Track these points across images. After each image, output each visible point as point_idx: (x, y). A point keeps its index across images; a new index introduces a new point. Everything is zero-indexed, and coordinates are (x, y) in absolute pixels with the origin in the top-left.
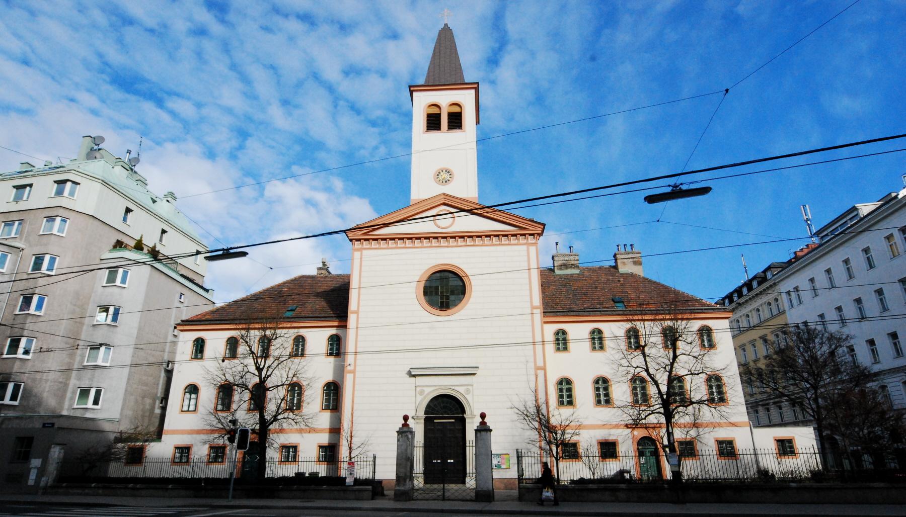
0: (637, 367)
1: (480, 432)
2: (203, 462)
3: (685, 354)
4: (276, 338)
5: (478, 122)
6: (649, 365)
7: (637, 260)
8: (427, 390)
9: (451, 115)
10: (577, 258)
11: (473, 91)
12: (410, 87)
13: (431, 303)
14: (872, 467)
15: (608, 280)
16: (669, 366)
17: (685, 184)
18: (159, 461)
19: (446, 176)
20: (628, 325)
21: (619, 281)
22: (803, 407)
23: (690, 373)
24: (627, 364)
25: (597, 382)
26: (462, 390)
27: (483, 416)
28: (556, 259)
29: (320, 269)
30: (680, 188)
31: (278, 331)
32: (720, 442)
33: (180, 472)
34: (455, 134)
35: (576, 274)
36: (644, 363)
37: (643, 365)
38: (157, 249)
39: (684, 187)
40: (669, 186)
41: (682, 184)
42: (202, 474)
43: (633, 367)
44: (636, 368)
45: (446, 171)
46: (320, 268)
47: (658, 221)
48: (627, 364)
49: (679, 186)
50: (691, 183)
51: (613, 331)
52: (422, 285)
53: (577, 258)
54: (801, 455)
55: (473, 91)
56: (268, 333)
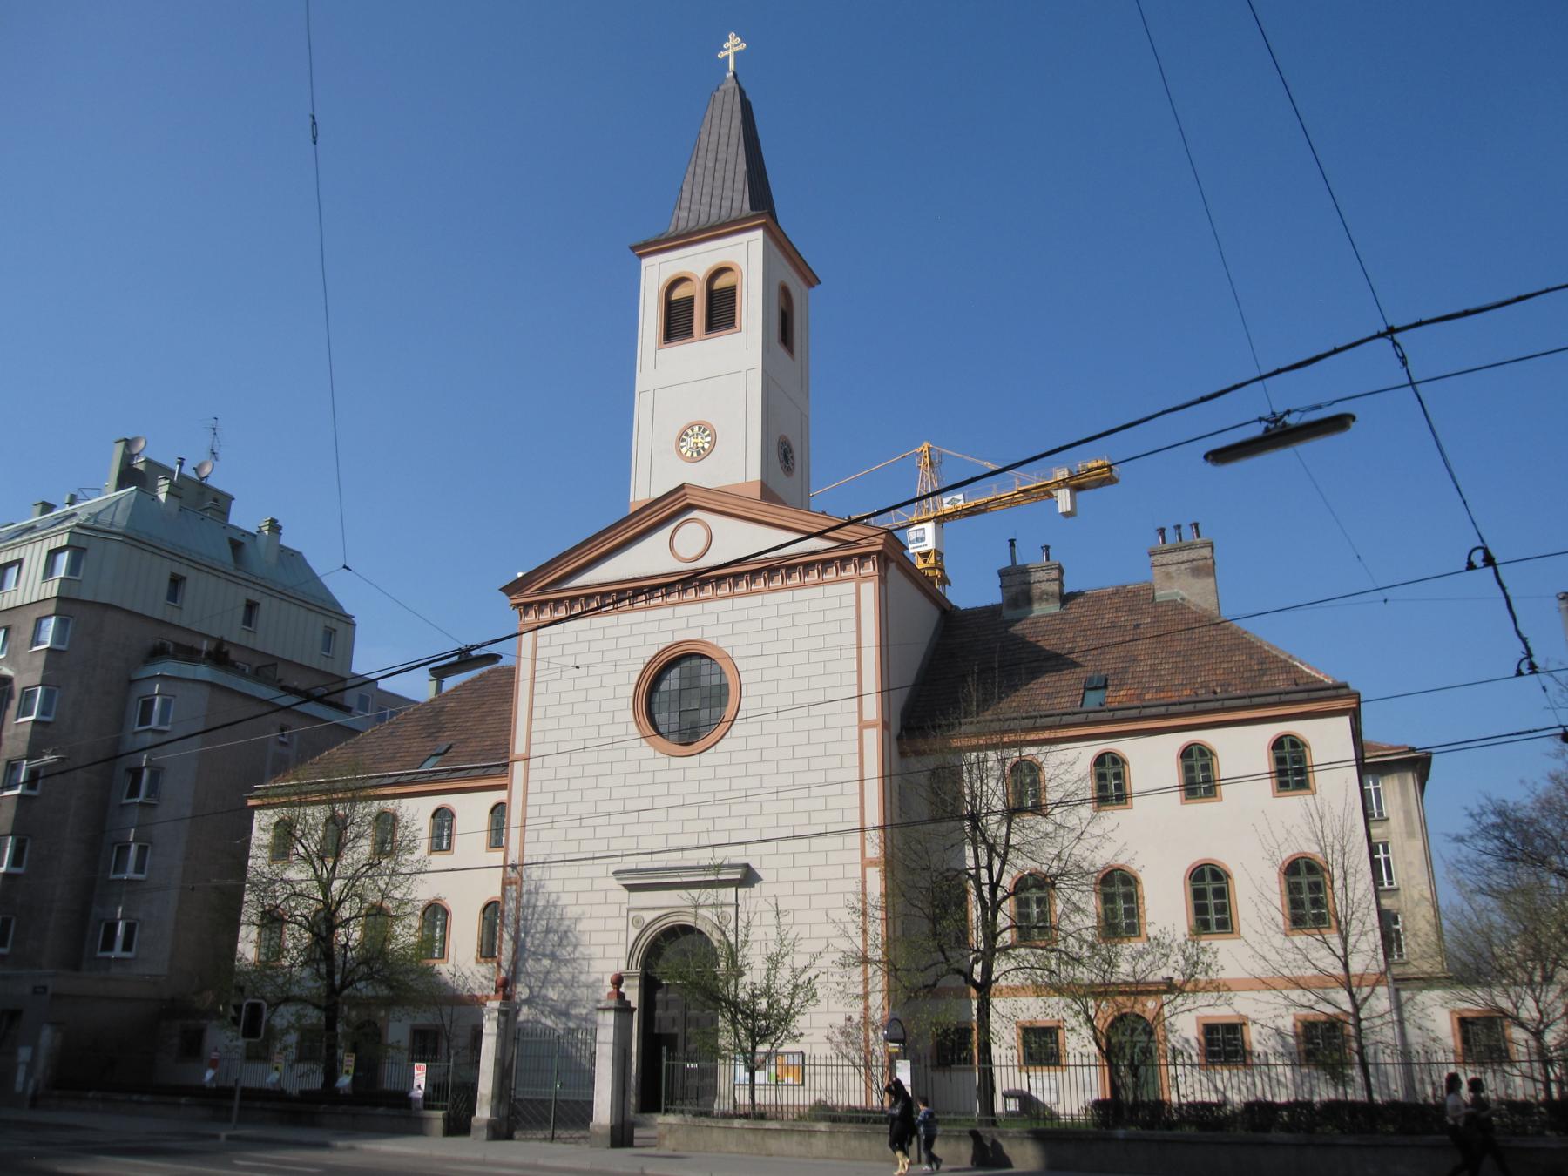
7: (1201, 562)
8: (649, 916)
9: (712, 295)
11: (1345, 721)
18: (818, 1062)
19: (703, 441)
32: (1210, 1030)
33: (829, 1078)
34: (722, 342)
39: (1292, 420)
40: (1260, 419)
41: (1288, 412)
49: (1282, 417)
54: (1072, 1069)
55: (1345, 721)
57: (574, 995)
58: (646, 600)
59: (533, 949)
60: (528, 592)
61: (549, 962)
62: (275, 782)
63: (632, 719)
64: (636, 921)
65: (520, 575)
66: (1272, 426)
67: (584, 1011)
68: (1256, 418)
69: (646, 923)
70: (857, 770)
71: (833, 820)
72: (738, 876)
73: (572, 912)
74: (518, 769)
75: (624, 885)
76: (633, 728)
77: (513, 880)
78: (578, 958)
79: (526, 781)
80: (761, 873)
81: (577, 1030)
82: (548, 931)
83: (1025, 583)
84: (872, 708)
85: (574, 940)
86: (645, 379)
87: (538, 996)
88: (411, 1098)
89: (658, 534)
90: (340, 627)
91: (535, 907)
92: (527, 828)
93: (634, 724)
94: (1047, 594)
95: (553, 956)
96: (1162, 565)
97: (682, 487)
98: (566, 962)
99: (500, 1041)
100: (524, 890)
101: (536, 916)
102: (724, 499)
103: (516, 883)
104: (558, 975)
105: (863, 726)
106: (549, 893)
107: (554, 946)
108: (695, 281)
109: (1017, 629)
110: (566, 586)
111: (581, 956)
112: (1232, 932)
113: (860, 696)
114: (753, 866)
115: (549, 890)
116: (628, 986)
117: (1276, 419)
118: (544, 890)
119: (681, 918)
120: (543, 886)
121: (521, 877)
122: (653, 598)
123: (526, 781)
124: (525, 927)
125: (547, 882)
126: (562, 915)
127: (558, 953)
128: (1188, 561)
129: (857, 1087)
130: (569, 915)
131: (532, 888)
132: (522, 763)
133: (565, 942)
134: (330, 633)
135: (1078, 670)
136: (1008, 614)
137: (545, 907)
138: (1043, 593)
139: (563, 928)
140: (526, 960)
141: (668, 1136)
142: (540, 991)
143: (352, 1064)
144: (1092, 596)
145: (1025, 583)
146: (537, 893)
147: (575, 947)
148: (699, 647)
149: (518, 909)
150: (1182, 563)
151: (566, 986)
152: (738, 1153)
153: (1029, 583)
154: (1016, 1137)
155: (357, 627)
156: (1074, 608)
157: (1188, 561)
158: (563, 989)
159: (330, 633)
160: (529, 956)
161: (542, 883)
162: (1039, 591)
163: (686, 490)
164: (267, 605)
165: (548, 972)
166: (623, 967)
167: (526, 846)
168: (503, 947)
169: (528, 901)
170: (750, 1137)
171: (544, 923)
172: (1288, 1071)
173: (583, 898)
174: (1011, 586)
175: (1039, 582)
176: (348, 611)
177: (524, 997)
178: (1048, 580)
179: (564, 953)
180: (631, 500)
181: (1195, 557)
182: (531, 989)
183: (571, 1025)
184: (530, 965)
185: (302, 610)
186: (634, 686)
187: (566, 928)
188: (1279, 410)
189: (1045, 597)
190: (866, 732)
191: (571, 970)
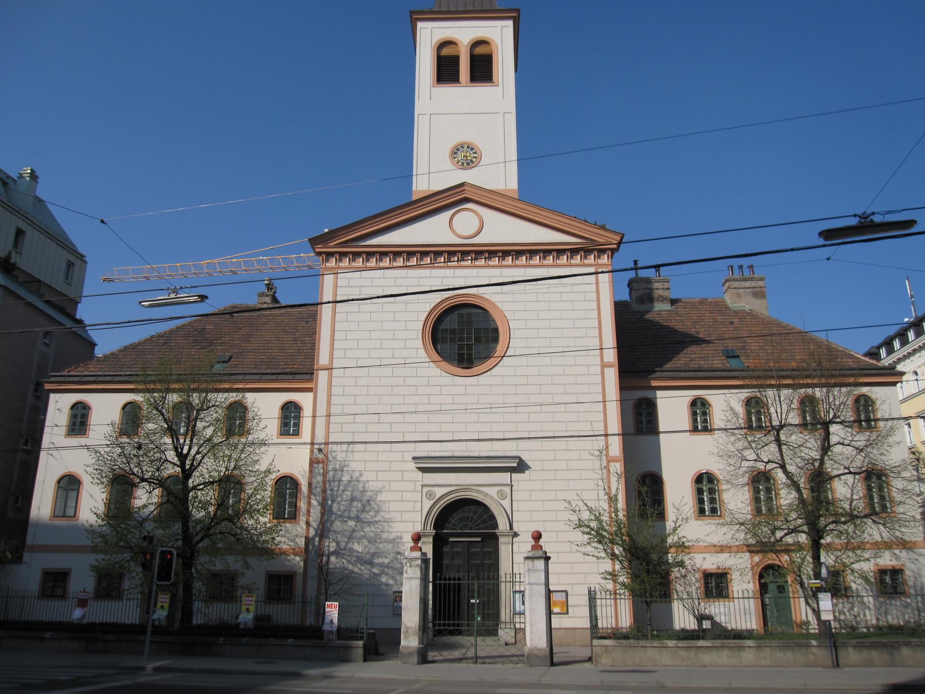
0: (769, 461)
1: (533, 561)
2: (31, 597)
3: (842, 444)
5: (516, 70)
7: (758, 290)
8: (440, 492)
9: (473, 58)
12: (412, 13)
13: (445, 356)
15: (715, 321)
16: (818, 461)
17: (877, 213)
20: (745, 394)
21: (732, 323)
23: (846, 471)
24: (754, 457)
25: (699, 479)
26: (493, 492)
27: (537, 536)
29: (262, 295)
30: (872, 219)
34: (481, 91)
35: (665, 311)
36: (778, 455)
38: (12, 261)
39: (877, 219)
40: (855, 216)
41: (873, 214)
42: (116, 616)
43: (763, 461)
44: (767, 463)
45: (468, 147)
48: (754, 457)
49: (869, 216)
50: (888, 212)
52: (500, 348)
56: (195, 399)
57: (378, 548)
58: (458, 261)
59: (339, 513)
60: (332, 244)
61: (354, 523)
62: (69, 372)
64: (430, 495)
65: (326, 230)
67: (386, 561)
69: (437, 497)
71: (586, 429)
73: (372, 486)
74: (322, 376)
76: (422, 353)
77: (320, 460)
78: (380, 521)
80: (529, 463)
81: (379, 575)
82: (353, 499)
83: (648, 289)
84: (611, 356)
85: (375, 507)
86: (421, 105)
87: (345, 549)
88: (323, 631)
89: (428, 220)
90: (77, 262)
91: (340, 481)
94: (662, 297)
95: (357, 519)
97: (462, 185)
98: (369, 523)
99: (422, 582)
100: (330, 468)
101: (341, 488)
102: (503, 200)
103: (323, 463)
104: (362, 533)
105: (604, 366)
106: (353, 471)
107: (358, 511)
108: (460, 45)
109: (648, 316)
110: (363, 244)
111: (382, 520)
112: (720, 516)
113: (601, 349)
114: (523, 458)
116: (423, 543)
118: (348, 469)
119: (467, 493)
120: (347, 466)
121: (327, 458)
122: (463, 260)
124: (332, 496)
125: (350, 463)
126: (364, 487)
127: (362, 516)
129: (609, 615)
130: (371, 488)
131: (337, 466)
132: (326, 372)
133: (367, 509)
134: (70, 265)
135: (711, 345)
136: (636, 307)
137: (349, 482)
138: (660, 296)
139: (366, 498)
140: (333, 522)
141: (604, 655)
142: (346, 545)
143: (168, 600)
144: (687, 303)
145: (648, 289)
146: (342, 471)
147: (378, 512)
149: (324, 482)
150: (747, 288)
151: (370, 542)
152: (672, 665)
154: (918, 646)
155: (88, 265)
156: (680, 307)
158: (367, 543)
159: (70, 265)
160: (336, 518)
161: (347, 463)
162: (657, 295)
163: (465, 188)
164: (31, 234)
165: (354, 531)
166: (418, 528)
168: (312, 511)
169: (334, 477)
170: (683, 653)
171: (349, 493)
172: (871, 599)
173: (381, 476)
174: (639, 289)
175: (657, 289)
176: (81, 250)
177: (332, 549)
178: (663, 289)
179: (367, 516)
180: (414, 188)
181: (754, 285)
182: (338, 543)
183: (375, 570)
184: (337, 525)
186: (422, 323)
187: (368, 498)
189: (663, 299)
191: (373, 529)
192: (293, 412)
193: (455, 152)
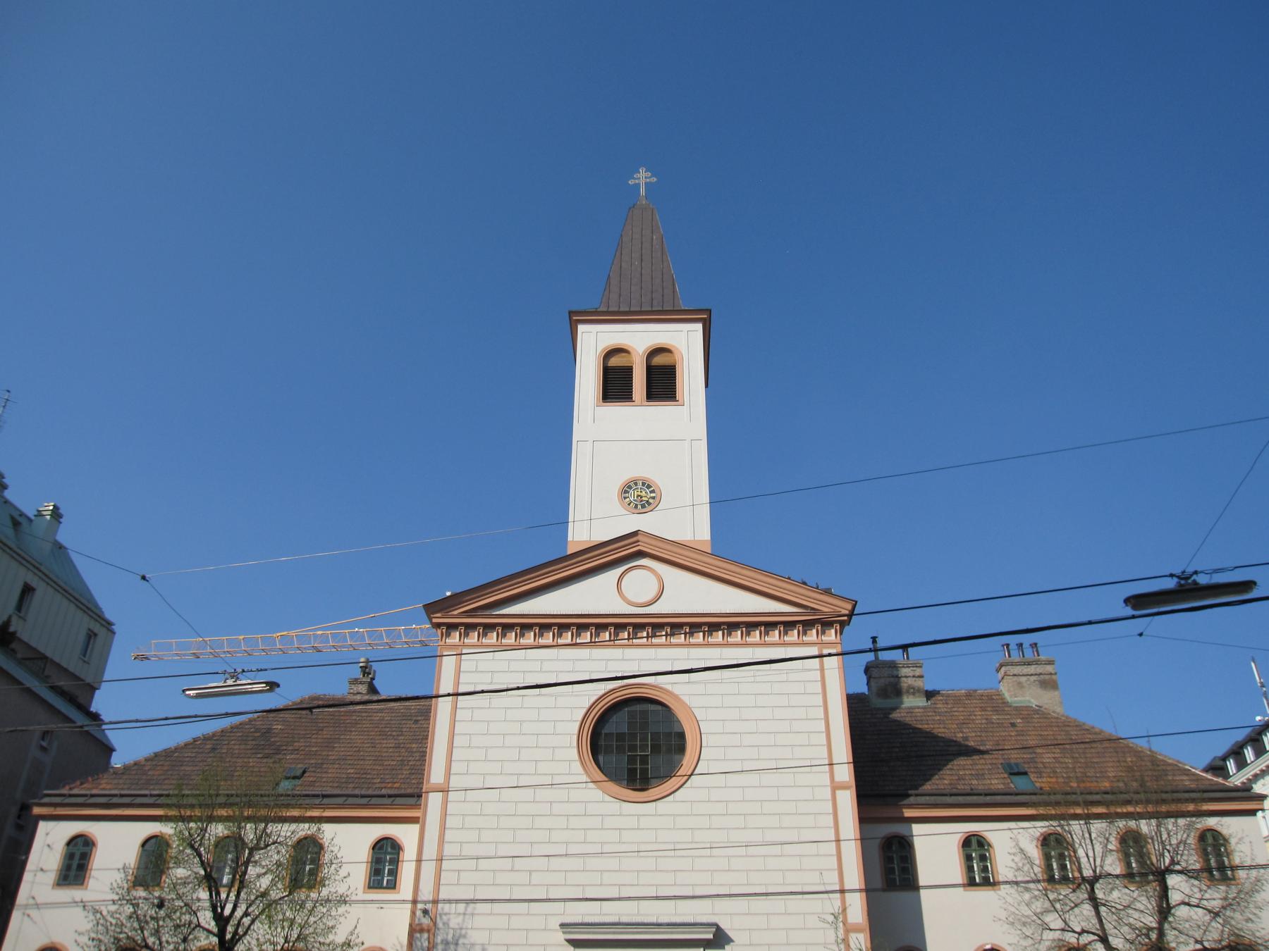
4: (267, 846)
5: (707, 386)
6: (1107, 926)
7: (1047, 677)
9: (651, 370)
10: (918, 672)
13: (612, 774)
14: (339, 937)
15: (990, 722)
17: (1202, 572)
20: (1040, 827)
21: (1013, 725)
22: (1141, 860)
24: (1060, 924)
28: (875, 672)
29: (355, 682)
30: (1194, 581)
31: (272, 828)
34: (661, 412)
35: (918, 708)
36: (1095, 921)
37: (1093, 924)
39: (1202, 580)
40: (1172, 575)
41: (1196, 573)
44: (1080, 934)
46: (356, 680)
47: (1141, 635)
48: (1060, 924)
49: (1192, 575)
50: (1217, 571)
51: (1022, 847)
53: (918, 672)
58: (648, 637)
60: (456, 612)
63: (576, 757)
65: (448, 594)
66: (1183, 582)
68: (1168, 573)
70: (833, 831)
72: (711, 936)
74: (434, 801)
75: (569, 941)
79: (444, 815)
80: (730, 934)
84: (845, 773)
90: (101, 632)
92: (445, 864)
93: (578, 764)
94: (914, 688)
96: (1014, 675)
97: (635, 533)
100: (439, 939)
105: (836, 787)
109: (895, 715)
110: (497, 613)
113: (831, 764)
115: (472, 941)
117: (1183, 577)
120: (464, 936)
121: (435, 924)
123: (444, 815)
125: (469, 932)
128: (1036, 675)
131: (450, 937)
134: (91, 635)
136: (878, 702)
138: (910, 687)
145: (893, 677)
146: (457, 944)
148: (668, 698)
150: (1032, 675)
153: (897, 677)
155: (116, 635)
157: (1036, 675)
159: (91, 635)
161: (463, 932)
164: (42, 592)
167: (441, 888)
174: (880, 678)
175: (906, 677)
178: (914, 676)
180: (570, 538)
185: (72, 605)
186: (578, 724)
188: (1190, 570)
189: (915, 691)
190: (839, 793)
192: (390, 854)
193: (626, 489)
